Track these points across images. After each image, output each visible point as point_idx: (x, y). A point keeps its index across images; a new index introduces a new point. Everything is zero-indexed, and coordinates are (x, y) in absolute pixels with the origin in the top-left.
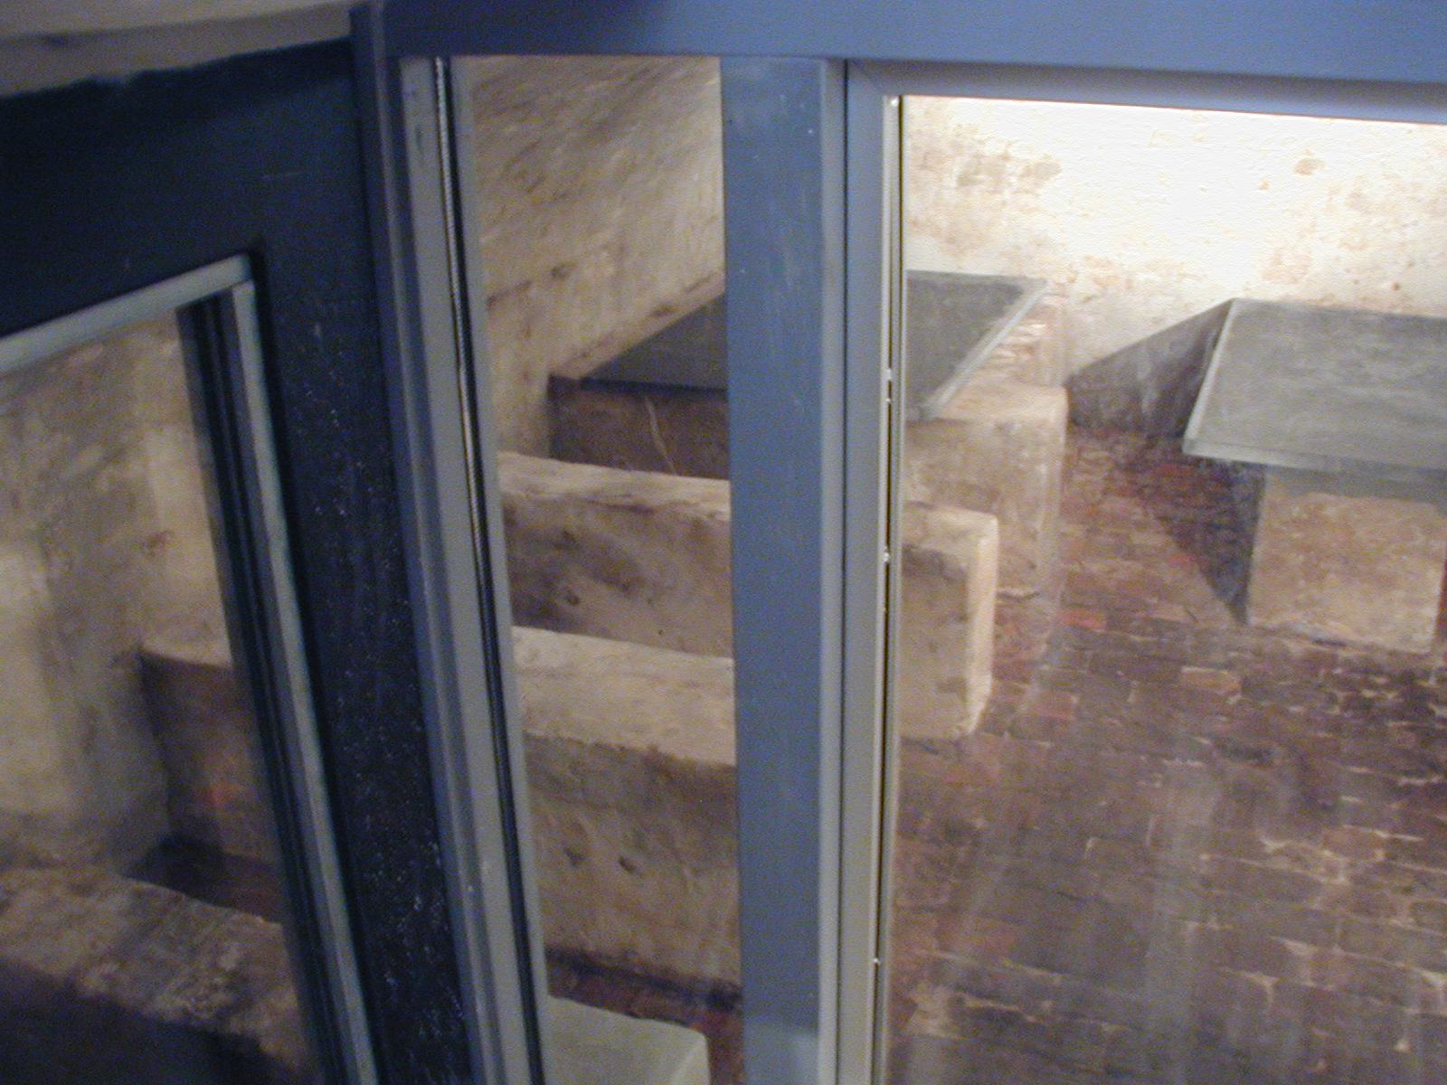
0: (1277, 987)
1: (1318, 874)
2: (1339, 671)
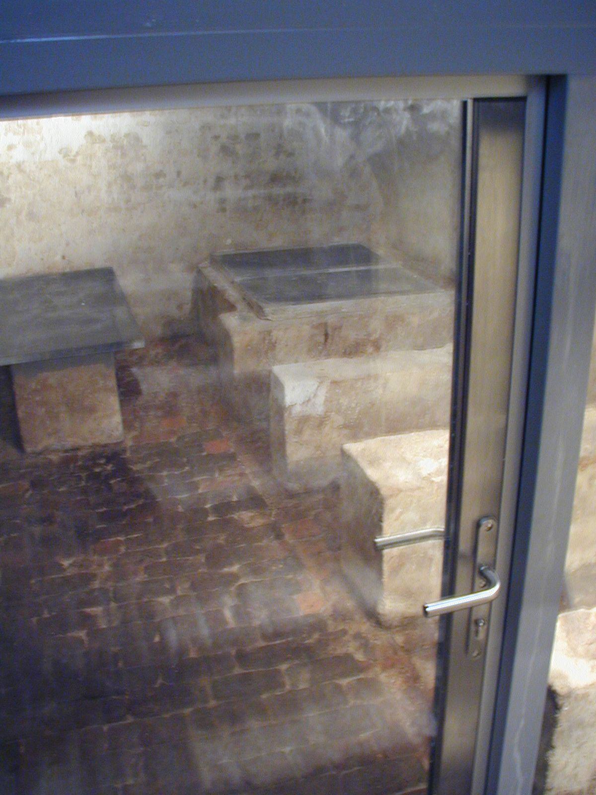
0: (88, 634)
1: (93, 569)
2: (80, 463)
